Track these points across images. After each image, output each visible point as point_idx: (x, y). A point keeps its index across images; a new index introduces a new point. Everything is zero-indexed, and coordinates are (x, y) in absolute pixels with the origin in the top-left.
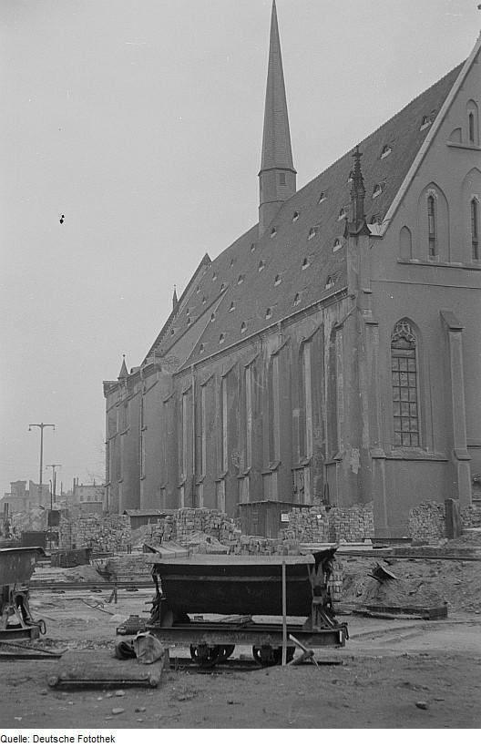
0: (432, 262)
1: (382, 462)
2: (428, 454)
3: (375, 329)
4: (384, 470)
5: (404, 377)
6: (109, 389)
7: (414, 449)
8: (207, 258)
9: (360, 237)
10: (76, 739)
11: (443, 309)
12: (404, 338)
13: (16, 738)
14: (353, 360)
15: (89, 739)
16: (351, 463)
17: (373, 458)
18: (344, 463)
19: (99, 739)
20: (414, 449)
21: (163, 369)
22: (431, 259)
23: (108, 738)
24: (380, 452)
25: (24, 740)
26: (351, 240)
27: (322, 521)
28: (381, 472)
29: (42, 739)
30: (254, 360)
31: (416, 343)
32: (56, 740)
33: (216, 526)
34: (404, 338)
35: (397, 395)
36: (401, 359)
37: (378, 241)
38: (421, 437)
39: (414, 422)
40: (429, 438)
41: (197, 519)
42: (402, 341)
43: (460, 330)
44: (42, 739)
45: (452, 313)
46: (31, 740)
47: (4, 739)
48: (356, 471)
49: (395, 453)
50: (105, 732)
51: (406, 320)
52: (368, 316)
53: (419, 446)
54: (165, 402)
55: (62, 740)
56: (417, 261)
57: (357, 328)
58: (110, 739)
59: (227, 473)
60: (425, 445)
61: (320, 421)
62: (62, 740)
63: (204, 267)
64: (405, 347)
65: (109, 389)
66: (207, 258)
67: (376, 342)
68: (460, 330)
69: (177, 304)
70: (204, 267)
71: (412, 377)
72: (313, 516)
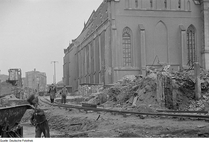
0: (136, 9)
1: (117, 71)
2: (134, 68)
3: (116, 31)
4: (118, 74)
5: (127, 45)
6: (65, 51)
7: (130, 67)
8: (94, 11)
9: (111, 2)
10: (22, 141)
11: (139, 24)
12: (127, 33)
13: (4, 141)
14: (110, 40)
15: (26, 141)
16: (109, 72)
17: (114, 70)
18: (106, 71)
19: (28, 141)
20: (130, 67)
21: (75, 45)
22: (136, 8)
23: (31, 141)
24: (117, 68)
25: (7, 141)
26: (109, 3)
27: (87, 89)
28: (117, 74)
29: (12, 141)
30: (91, 41)
31: (131, 34)
32: (16, 141)
33: (19, 92)
34: (127, 33)
35: (124, 51)
36: (126, 40)
37: (118, 3)
38: (132, 63)
39: (130, 59)
40: (134, 64)
41: (15, 90)
42: (126, 34)
43: (144, 30)
44: (12, 141)
45: (142, 25)
46: (9, 141)
47: (1, 141)
48: (110, 74)
49: (123, 68)
50: (30, 139)
51: (127, 27)
52: (113, 27)
53: (131, 66)
54: (75, 55)
55: (18, 141)
56: (131, 9)
57: (110, 30)
58: (32, 141)
59: (86, 75)
60: (133, 65)
61: (103, 60)
62: (18, 141)
63: (93, 14)
64: (127, 36)
65: (65, 51)
66: (94, 11)
67: (116, 35)
68: (144, 30)
69: (85, 25)
70: (93, 14)
71: (129, 45)
72: (84, 88)
